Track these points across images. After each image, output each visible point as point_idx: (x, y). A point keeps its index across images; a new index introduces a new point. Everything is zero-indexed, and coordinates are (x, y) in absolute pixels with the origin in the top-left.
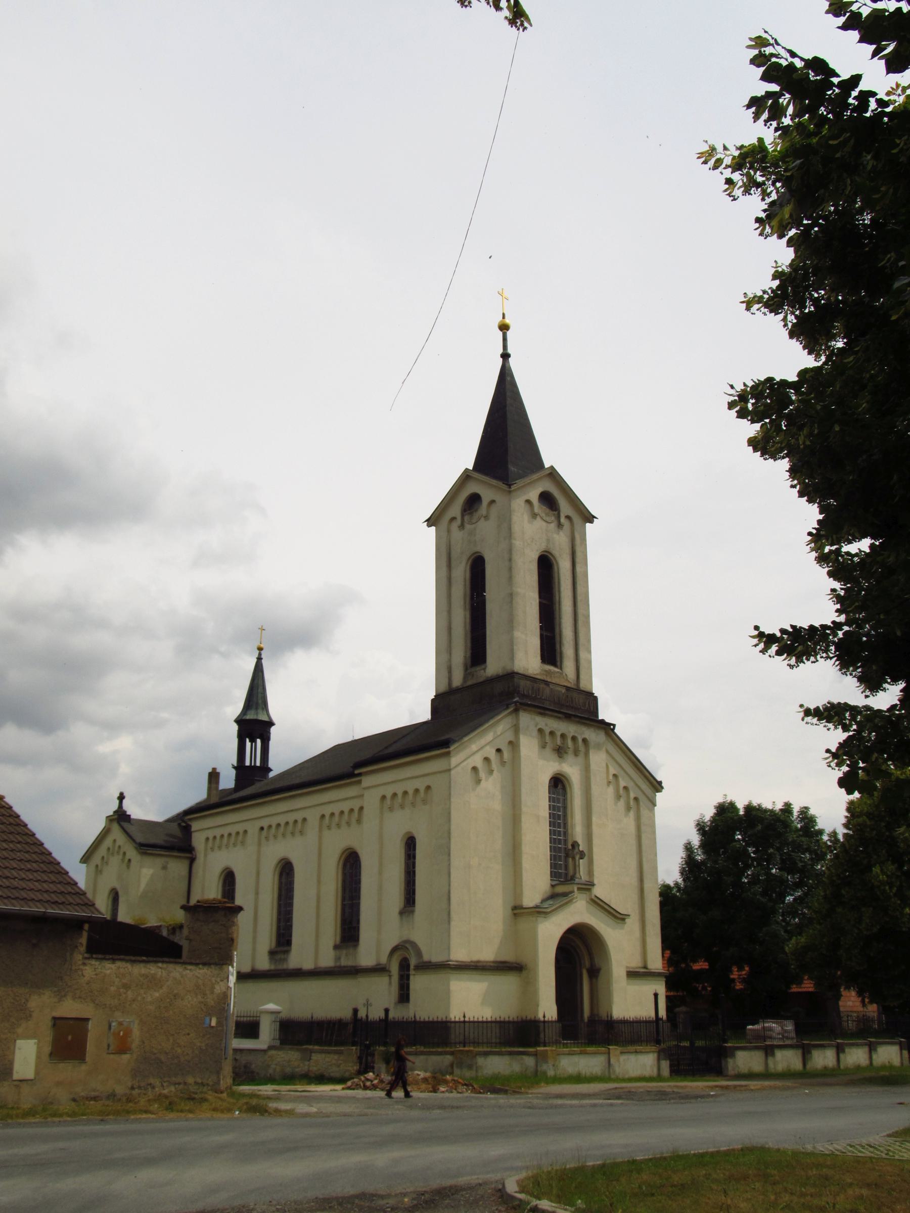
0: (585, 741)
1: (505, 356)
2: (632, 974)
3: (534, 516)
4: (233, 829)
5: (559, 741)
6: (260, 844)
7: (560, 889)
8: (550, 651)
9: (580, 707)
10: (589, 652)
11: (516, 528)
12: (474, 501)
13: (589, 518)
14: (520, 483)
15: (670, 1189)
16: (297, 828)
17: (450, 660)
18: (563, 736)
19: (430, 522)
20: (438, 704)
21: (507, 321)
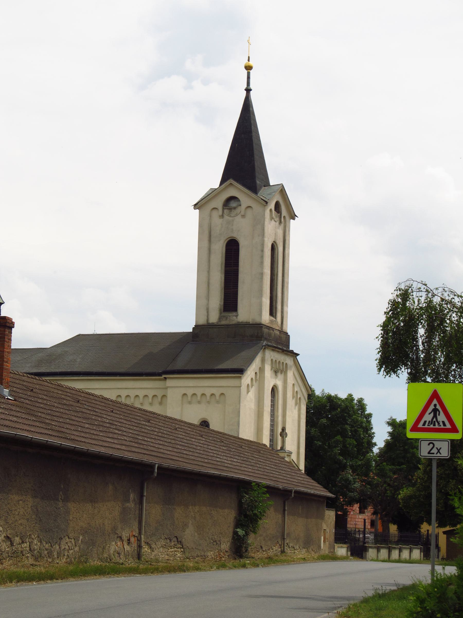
1: (248, 90)
10: (287, 306)
13: (293, 216)
17: (208, 304)
19: (196, 206)
20: (197, 327)
21: (251, 63)
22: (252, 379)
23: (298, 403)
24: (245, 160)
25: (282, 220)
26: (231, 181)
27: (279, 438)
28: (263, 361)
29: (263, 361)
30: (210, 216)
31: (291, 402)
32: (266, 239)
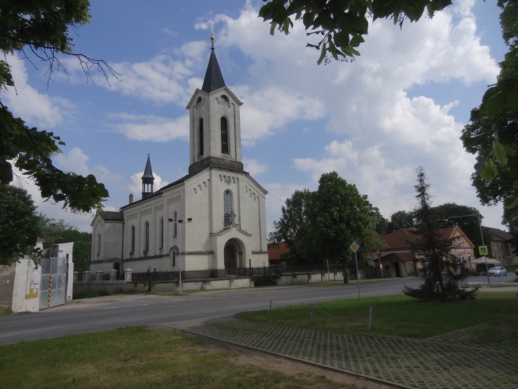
0: (237, 178)
2: (254, 253)
3: (219, 103)
4: (134, 213)
5: (227, 179)
6: (140, 217)
7: (227, 227)
8: (225, 149)
9: (237, 168)
11: (212, 107)
12: (200, 99)
14: (212, 92)
16: (149, 211)
18: (229, 177)
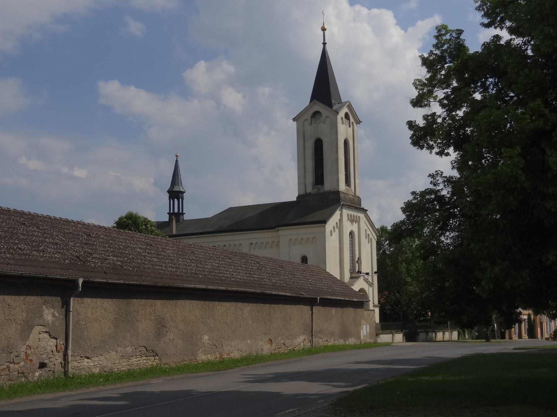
1: (324, 44)
15: (138, 250)
19: (294, 119)
20: (299, 197)
22: (334, 227)
23: (370, 241)
24: (324, 87)
25: (351, 124)
26: (315, 101)
27: (357, 264)
28: (341, 215)
29: (341, 215)
30: (304, 125)
31: (364, 241)
32: (339, 137)
